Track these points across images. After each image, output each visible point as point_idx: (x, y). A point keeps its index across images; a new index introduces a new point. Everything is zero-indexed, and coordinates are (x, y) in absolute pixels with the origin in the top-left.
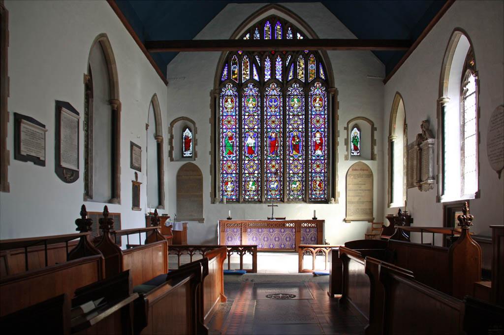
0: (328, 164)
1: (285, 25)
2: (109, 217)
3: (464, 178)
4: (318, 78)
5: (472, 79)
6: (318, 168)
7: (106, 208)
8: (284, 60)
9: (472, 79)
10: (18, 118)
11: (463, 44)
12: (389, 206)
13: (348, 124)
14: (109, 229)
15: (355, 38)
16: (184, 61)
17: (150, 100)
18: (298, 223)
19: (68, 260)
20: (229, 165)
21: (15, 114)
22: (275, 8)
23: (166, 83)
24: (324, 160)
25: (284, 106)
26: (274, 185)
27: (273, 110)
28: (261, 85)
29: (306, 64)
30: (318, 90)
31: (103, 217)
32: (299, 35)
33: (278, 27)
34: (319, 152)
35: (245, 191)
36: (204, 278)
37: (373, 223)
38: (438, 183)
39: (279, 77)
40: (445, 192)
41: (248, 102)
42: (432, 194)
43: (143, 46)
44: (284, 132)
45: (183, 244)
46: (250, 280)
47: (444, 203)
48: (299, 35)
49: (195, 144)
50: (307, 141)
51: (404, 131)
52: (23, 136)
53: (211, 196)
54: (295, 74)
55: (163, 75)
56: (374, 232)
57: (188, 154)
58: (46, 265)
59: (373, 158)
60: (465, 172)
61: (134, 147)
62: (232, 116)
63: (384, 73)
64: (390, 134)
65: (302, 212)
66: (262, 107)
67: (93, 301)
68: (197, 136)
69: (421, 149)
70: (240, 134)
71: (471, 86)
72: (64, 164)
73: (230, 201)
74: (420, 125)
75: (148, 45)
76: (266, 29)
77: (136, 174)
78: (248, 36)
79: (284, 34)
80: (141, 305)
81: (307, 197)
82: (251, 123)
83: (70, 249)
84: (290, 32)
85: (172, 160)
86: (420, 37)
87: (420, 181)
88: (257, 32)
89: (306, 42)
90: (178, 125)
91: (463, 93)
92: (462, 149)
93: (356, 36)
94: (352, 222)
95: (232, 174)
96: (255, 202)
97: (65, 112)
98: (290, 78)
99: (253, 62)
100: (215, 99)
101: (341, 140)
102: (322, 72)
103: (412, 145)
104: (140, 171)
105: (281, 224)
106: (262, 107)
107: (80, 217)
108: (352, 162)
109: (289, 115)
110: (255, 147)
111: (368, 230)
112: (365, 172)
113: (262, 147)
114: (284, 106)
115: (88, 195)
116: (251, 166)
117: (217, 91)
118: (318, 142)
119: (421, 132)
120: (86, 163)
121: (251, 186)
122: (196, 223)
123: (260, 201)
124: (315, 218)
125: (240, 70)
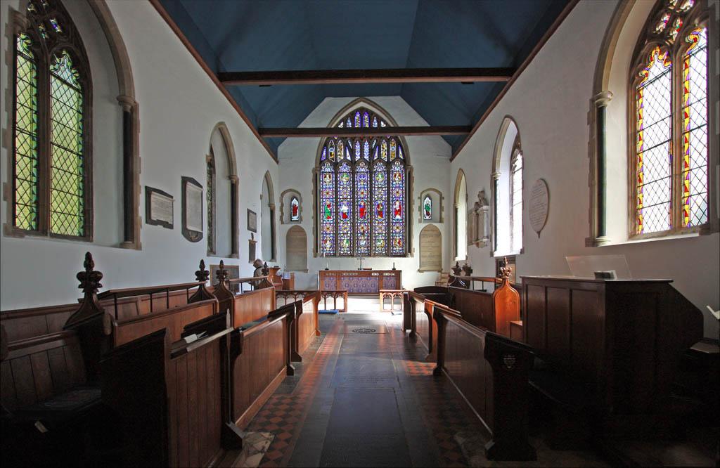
0: (405, 226)
1: (371, 114)
2: (225, 269)
3: (513, 237)
4: (398, 157)
5: (519, 157)
6: (398, 229)
7: (222, 262)
8: (370, 144)
9: (519, 157)
10: (149, 191)
11: (511, 130)
12: (454, 259)
13: (422, 193)
14: (224, 279)
15: (429, 125)
16: (290, 145)
17: (264, 175)
18: (381, 272)
19: (188, 303)
20: (328, 228)
21: (146, 187)
22: (364, 101)
23: (277, 162)
24: (403, 222)
25: (371, 181)
26: (362, 243)
27: (361, 184)
28: (353, 164)
29: (388, 147)
30: (397, 168)
31: (219, 269)
32: (382, 123)
33: (366, 117)
34: (398, 217)
35: (341, 247)
36: (298, 317)
37: (442, 273)
38: (491, 241)
39: (366, 157)
40: (498, 247)
41: (342, 177)
42: (486, 250)
43: (257, 133)
44: (371, 202)
45: (291, 289)
46: (341, 317)
47: (496, 257)
48: (382, 123)
49: (301, 211)
50: (389, 208)
51: (467, 199)
52: (153, 205)
53: (314, 251)
54: (380, 154)
55: (275, 155)
56: (442, 281)
57: (295, 218)
58: (168, 307)
59: (441, 221)
60: (514, 232)
61: (251, 213)
62: (330, 188)
63: (450, 152)
64: (455, 202)
65: (386, 264)
66: (354, 181)
67: (197, 334)
68: (302, 205)
69: (478, 214)
70: (336, 203)
71: (519, 163)
72: (189, 227)
73: (327, 255)
74: (219, 121)
75: (261, 132)
76: (356, 118)
77: (252, 234)
78: (342, 124)
79: (370, 123)
80: (236, 335)
81: (389, 253)
82: (345, 194)
83: (190, 296)
84: (375, 121)
85: (282, 223)
86: (479, 123)
87: (478, 239)
88: (349, 121)
89: (388, 129)
90: (288, 195)
91: (512, 169)
92: (511, 214)
93: (429, 123)
94: (425, 273)
95: (330, 234)
96: (348, 256)
97: (190, 186)
98: (375, 158)
99: (346, 145)
100: (316, 175)
101: (415, 207)
102: (400, 153)
103: (471, 211)
104: (256, 232)
105: (368, 273)
106: (354, 181)
107: (199, 270)
108: (423, 225)
109: (375, 188)
110: (348, 213)
111: (438, 279)
112: (435, 233)
113: (354, 213)
114: (371, 181)
115: (211, 251)
116: (345, 227)
117: (318, 169)
118: (398, 209)
119: (478, 201)
120: (210, 225)
121: (345, 244)
122: (302, 273)
123: (352, 256)
124: (394, 269)
125: (336, 152)
